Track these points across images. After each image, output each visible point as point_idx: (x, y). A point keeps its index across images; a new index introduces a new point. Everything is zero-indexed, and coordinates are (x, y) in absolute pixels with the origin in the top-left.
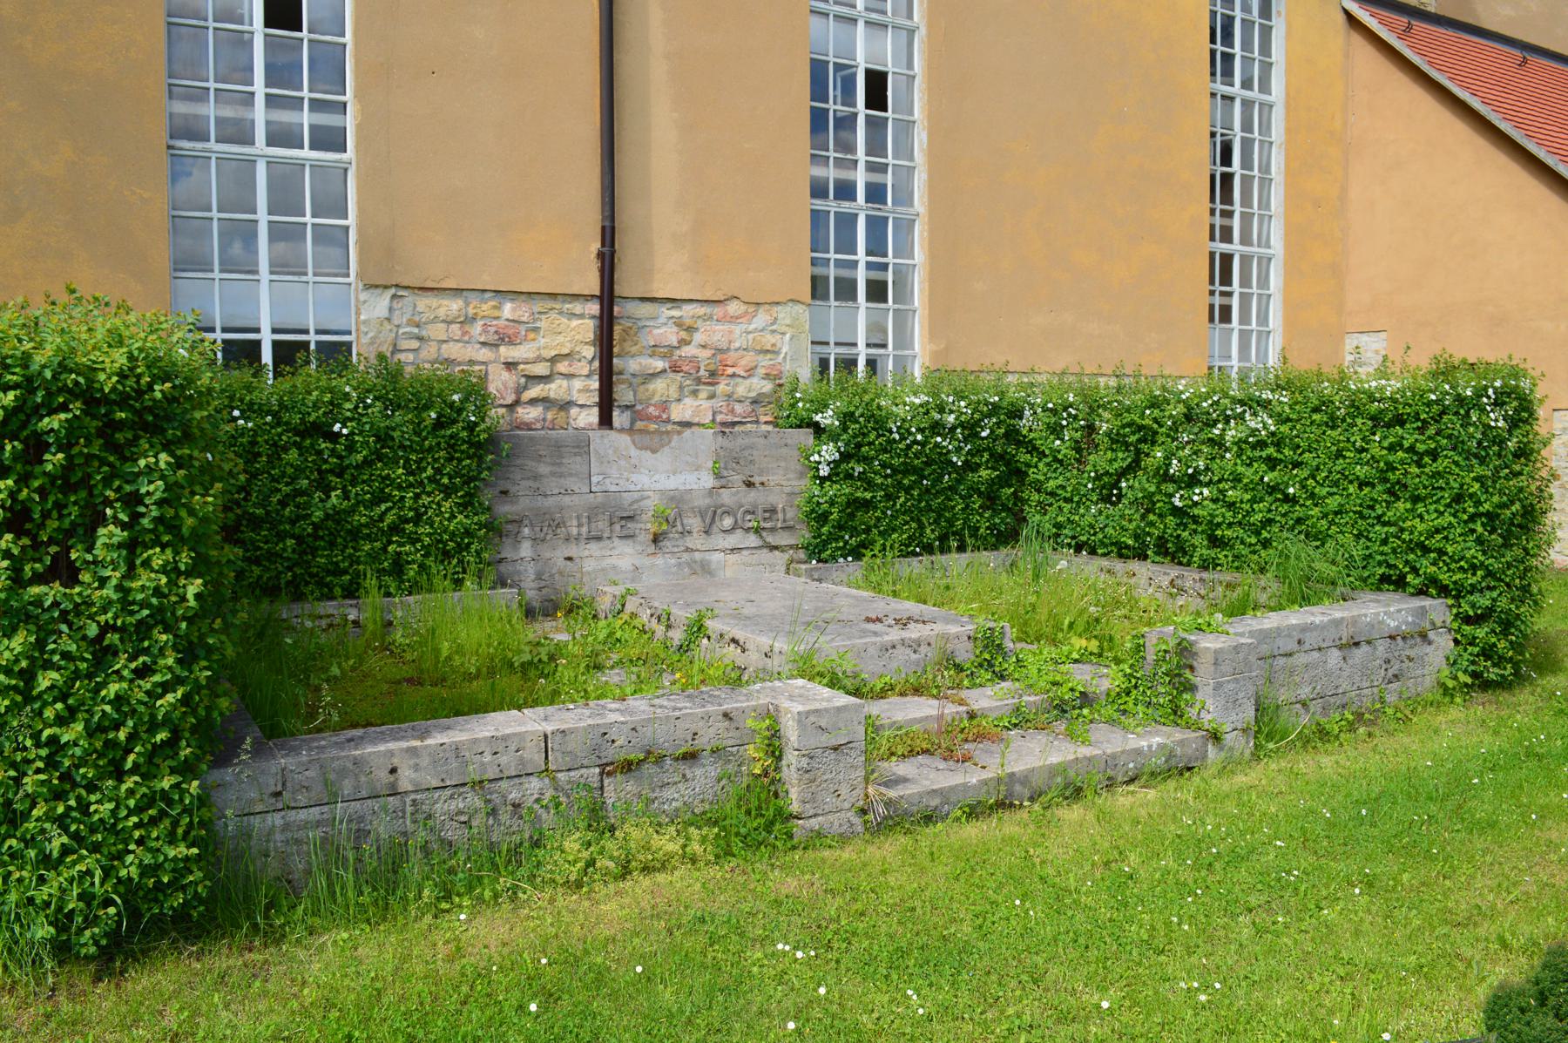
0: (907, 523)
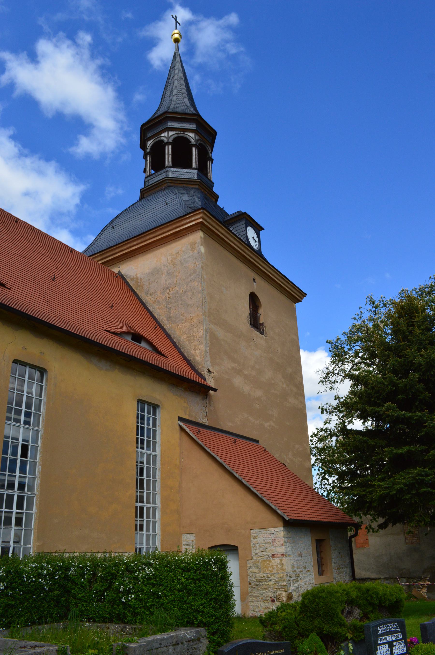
0: (26, 613)
